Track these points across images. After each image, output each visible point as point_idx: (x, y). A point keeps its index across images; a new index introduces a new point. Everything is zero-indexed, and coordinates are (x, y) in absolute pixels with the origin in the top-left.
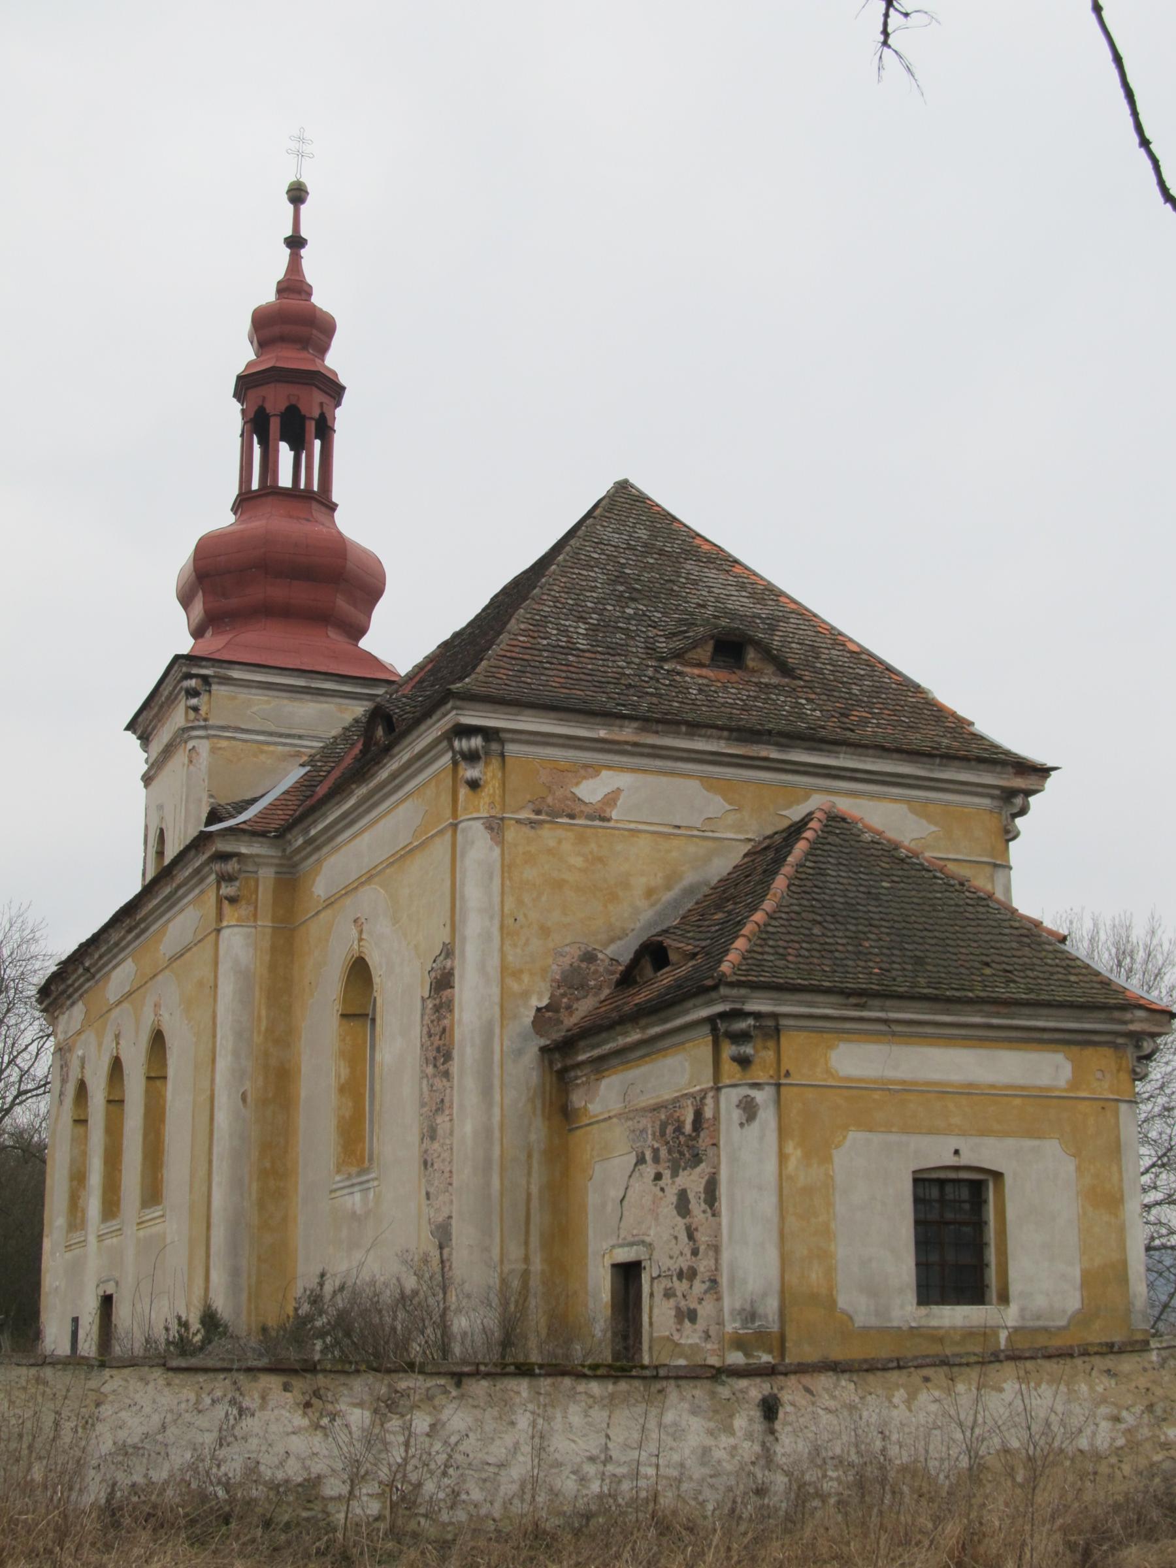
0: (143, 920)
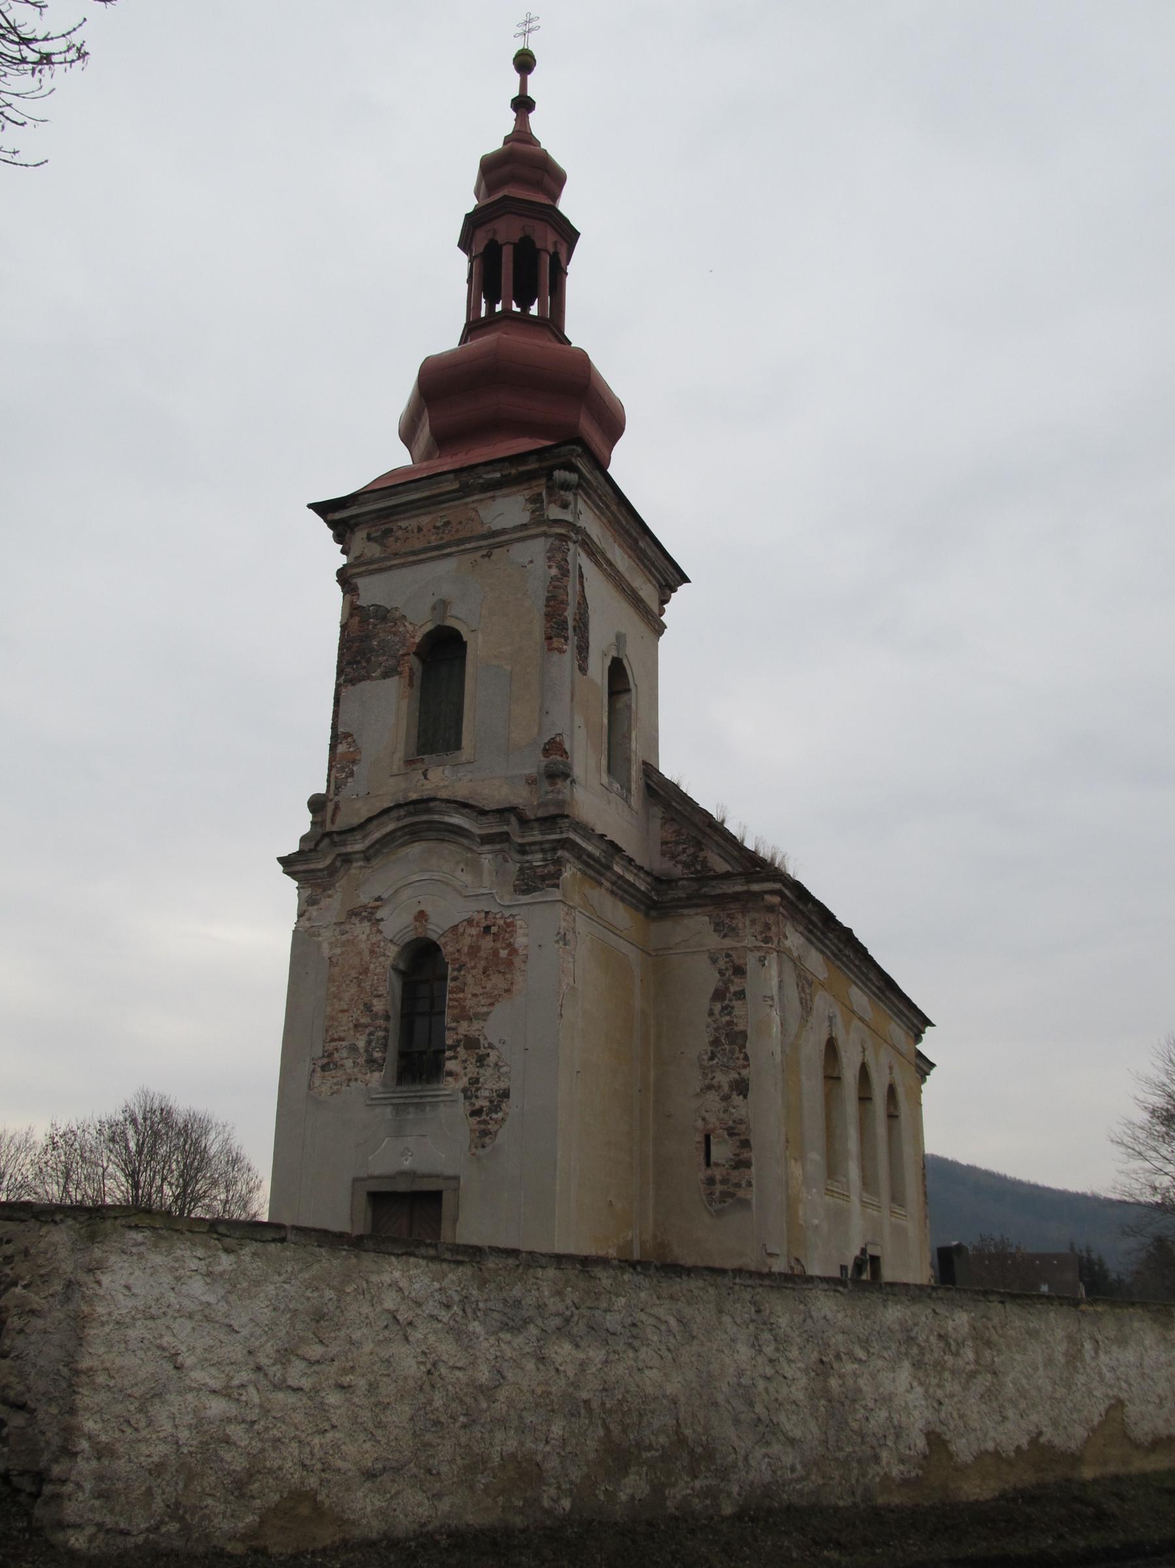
0: (889, 999)
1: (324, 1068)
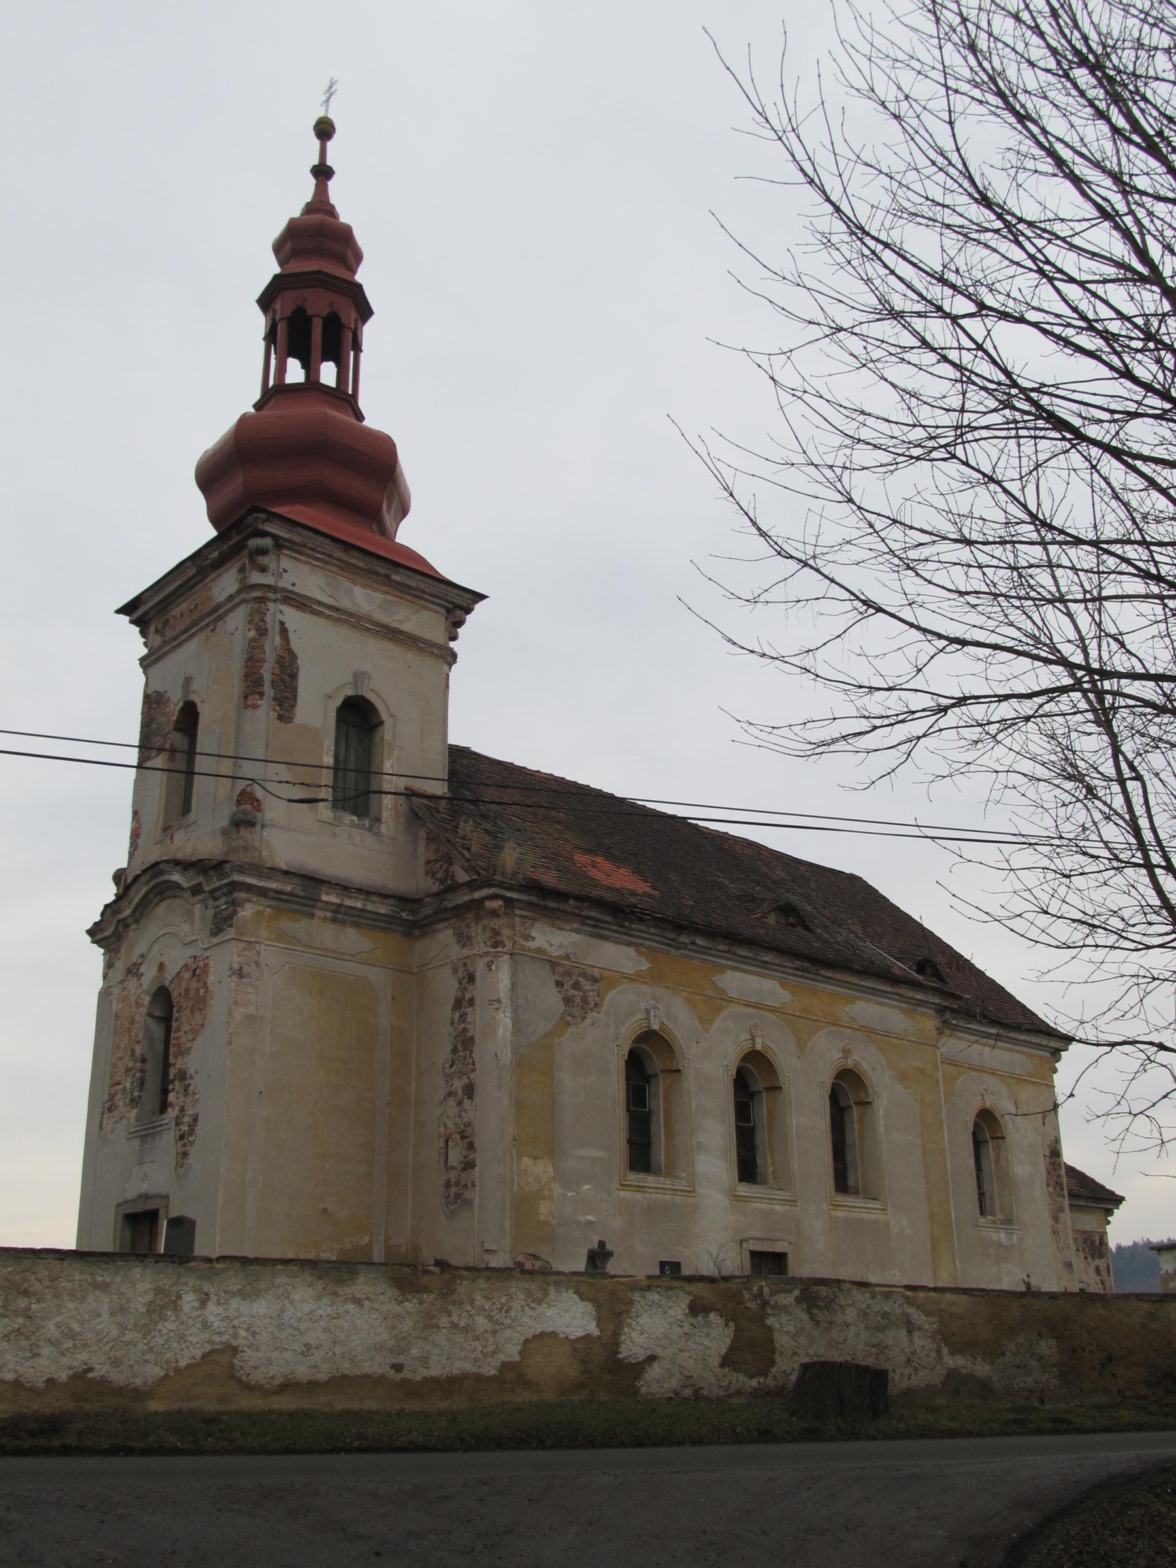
1: (110, 1110)
